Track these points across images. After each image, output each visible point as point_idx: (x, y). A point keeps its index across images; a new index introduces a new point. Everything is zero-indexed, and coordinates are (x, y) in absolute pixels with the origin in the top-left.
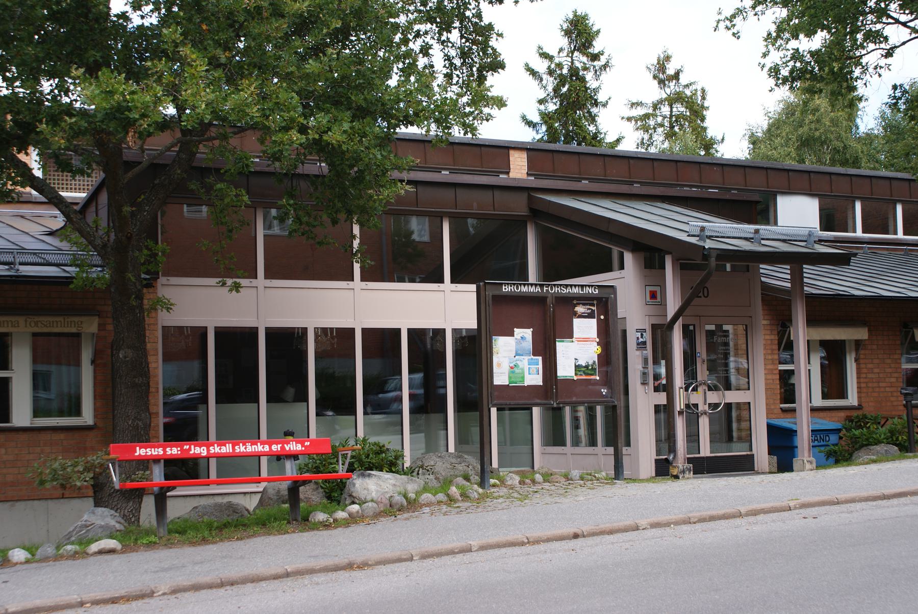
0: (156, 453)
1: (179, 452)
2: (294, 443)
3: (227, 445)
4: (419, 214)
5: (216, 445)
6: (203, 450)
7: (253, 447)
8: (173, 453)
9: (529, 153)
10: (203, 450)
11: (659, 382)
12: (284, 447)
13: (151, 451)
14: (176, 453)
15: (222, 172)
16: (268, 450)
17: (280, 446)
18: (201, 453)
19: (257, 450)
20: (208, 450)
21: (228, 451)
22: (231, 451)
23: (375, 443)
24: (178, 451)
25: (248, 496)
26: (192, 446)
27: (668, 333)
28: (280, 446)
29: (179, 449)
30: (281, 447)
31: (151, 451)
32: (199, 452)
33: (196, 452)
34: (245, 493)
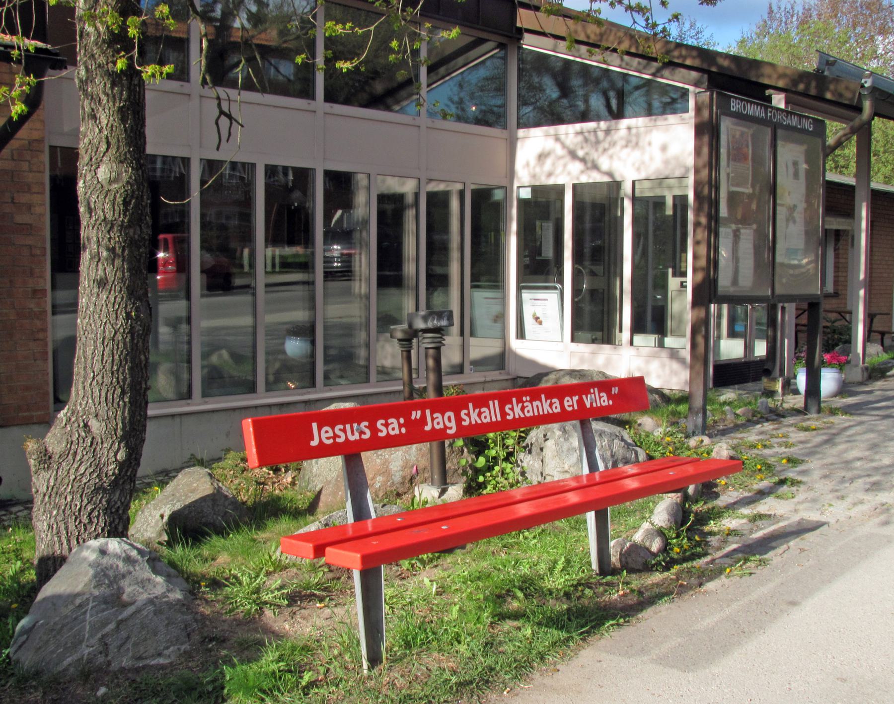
0: (357, 436)
1: (404, 430)
2: (596, 390)
3: (491, 403)
4: (778, 109)
5: (471, 405)
6: (449, 419)
7: (535, 403)
8: (392, 433)
9: (788, 94)
10: (449, 419)
11: (345, 252)
12: (582, 398)
13: (344, 430)
14: (397, 432)
15: (218, 24)
16: (559, 410)
17: (576, 398)
18: (446, 427)
19: (541, 413)
20: (459, 420)
21: (494, 419)
22: (499, 419)
23: (600, 372)
24: (400, 426)
25: (177, 420)
26: (428, 412)
27: (683, 255)
28: (576, 398)
29: (402, 421)
30: (577, 401)
31: (344, 430)
32: (441, 426)
33: (437, 427)
34: (173, 416)
